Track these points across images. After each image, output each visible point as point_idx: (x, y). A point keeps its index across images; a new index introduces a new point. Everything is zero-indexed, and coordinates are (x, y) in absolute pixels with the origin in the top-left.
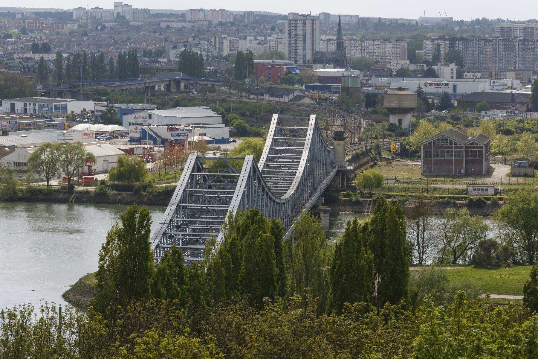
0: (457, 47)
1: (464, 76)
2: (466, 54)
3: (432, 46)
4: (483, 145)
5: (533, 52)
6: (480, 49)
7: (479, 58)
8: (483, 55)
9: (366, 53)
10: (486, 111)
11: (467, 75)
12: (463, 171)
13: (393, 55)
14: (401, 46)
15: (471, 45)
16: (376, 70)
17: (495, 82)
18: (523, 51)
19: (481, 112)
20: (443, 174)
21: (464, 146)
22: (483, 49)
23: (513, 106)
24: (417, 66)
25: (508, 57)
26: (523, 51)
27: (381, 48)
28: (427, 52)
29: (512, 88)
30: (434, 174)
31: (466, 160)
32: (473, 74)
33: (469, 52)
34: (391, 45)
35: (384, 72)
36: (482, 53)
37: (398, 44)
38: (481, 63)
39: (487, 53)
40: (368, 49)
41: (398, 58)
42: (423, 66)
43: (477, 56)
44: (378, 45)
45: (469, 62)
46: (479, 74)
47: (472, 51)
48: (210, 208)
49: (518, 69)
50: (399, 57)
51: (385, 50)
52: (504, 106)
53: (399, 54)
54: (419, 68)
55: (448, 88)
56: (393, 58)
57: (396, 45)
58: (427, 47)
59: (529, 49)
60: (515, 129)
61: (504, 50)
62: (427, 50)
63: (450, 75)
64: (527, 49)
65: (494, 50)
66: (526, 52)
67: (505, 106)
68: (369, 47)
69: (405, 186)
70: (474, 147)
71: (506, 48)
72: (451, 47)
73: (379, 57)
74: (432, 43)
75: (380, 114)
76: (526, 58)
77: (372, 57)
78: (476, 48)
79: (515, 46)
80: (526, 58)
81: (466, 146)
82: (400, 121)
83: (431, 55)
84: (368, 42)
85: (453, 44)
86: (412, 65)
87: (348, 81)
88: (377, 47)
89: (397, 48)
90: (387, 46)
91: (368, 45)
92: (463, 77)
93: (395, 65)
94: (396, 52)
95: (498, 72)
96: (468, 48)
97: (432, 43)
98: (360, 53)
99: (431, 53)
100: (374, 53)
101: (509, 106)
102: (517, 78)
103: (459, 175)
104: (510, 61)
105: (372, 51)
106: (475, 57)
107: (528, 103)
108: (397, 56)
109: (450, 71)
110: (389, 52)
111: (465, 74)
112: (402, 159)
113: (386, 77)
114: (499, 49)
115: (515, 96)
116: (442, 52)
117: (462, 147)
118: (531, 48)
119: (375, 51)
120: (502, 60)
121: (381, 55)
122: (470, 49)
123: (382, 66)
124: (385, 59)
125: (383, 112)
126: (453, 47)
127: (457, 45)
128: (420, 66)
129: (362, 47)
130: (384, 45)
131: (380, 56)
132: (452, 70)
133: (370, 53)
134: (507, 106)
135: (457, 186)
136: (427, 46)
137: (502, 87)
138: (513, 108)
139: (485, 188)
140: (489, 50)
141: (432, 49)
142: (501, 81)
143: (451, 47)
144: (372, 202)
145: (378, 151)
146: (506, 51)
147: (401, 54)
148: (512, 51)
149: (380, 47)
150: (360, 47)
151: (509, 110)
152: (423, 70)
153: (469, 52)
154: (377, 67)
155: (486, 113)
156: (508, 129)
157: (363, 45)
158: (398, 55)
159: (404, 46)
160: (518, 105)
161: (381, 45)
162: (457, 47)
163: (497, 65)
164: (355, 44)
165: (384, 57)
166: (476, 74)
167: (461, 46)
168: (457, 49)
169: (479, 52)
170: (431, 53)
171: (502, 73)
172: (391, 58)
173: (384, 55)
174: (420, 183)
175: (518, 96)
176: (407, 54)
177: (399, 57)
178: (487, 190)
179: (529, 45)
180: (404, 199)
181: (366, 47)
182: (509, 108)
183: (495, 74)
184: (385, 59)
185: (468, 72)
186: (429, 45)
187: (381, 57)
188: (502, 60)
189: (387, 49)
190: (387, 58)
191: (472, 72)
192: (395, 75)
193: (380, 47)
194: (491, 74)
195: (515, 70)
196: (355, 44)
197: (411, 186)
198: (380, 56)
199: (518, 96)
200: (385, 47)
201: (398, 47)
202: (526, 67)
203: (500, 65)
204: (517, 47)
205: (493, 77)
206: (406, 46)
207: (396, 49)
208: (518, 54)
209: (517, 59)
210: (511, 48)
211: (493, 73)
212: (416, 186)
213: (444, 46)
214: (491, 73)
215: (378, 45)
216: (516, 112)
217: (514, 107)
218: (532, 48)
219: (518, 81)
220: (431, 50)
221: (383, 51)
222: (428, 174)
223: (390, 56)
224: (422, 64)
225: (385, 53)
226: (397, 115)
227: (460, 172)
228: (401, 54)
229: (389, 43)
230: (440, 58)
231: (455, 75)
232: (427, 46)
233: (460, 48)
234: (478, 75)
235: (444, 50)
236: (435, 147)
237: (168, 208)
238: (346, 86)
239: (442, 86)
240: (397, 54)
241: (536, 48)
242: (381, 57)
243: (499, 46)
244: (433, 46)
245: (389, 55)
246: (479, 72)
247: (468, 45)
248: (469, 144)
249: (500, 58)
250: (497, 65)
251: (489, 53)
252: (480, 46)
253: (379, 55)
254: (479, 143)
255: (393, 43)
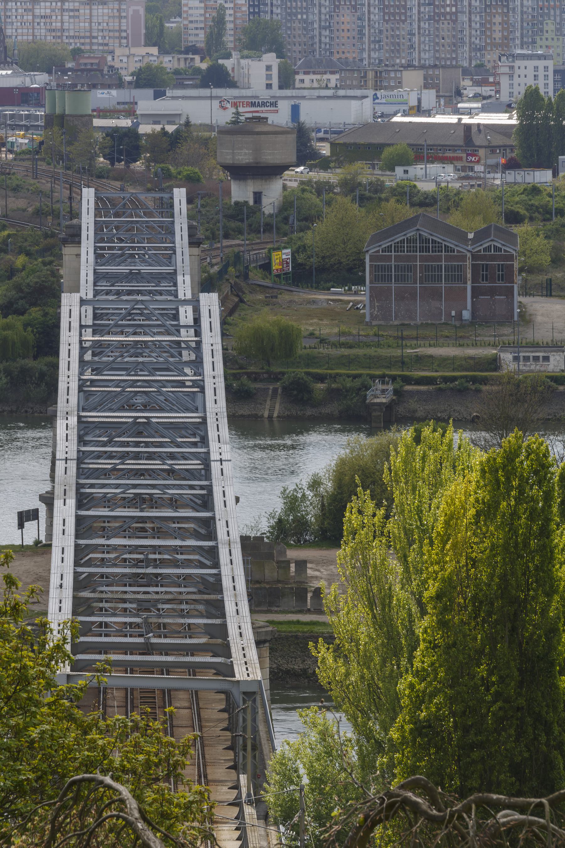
0: (267, 12)
1: (297, 82)
2: (290, 28)
3: (202, 12)
4: (514, 253)
5: (455, 21)
6: (323, 17)
7: (323, 39)
8: (331, 31)
9: (43, 31)
10: (406, 168)
11: (302, 81)
12: (466, 315)
13: (111, 34)
14: (131, 13)
15: (301, 8)
16: (82, 71)
17: (379, 96)
18: (429, 19)
19: (393, 170)
20: (419, 322)
21: (469, 255)
22: (331, 16)
23: (468, 155)
24: (179, 59)
25: (392, 36)
26: (429, 19)
27: (82, 18)
28: (191, 26)
29: (419, 110)
30: (396, 323)
31: (473, 288)
32: (318, 77)
33: (296, 25)
34: (106, 11)
35: (103, 75)
36: (330, 26)
37: (124, 7)
38: (326, 50)
39: (343, 27)
40: (48, 20)
41: (124, 41)
42: (192, 59)
43: (316, 32)
44: (72, 10)
45: (298, 48)
46: (334, 79)
47: (305, 21)
48: (154, 420)
49: (417, 64)
50: (125, 38)
51: (91, 22)
52: (446, 155)
53: (126, 31)
54: (182, 65)
55: (277, 111)
56: (111, 41)
57: (119, 10)
58: (191, 15)
59: (444, 15)
60: (527, 210)
61: (384, 20)
62: (191, 22)
63: (264, 82)
64: (439, 15)
65: (359, 19)
66: (438, 22)
67: (449, 154)
68: (51, 17)
69: (345, 352)
70: (493, 258)
71: (389, 14)
72: (254, 13)
73: (77, 41)
74: (202, 5)
75: (177, 178)
76: (437, 36)
77: (59, 41)
78: (313, 14)
79: (411, 9)
80: (437, 36)
81: (472, 255)
82: (258, 197)
83: (202, 36)
84: (48, 4)
85: (258, 6)
86: (167, 58)
87: (63, 98)
88: (70, 17)
89: (120, 17)
90: (95, 13)
91: (48, 11)
92: (294, 84)
93: (125, 60)
94: (117, 28)
95: (381, 72)
96: (296, 15)
97: (202, 5)
98: (31, 31)
99: (201, 28)
100: (63, 30)
101: (459, 154)
102: (426, 87)
103: (458, 324)
104: (399, 45)
105: (59, 24)
106: (312, 38)
107: (512, 148)
108: (120, 38)
109: (264, 72)
110: (100, 28)
111: (298, 77)
112: (298, 286)
113: (109, 87)
114: (372, 17)
115: (474, 130)
116: (230, 26)
117: (463, 258)
118: (448, 13)
119: (66, 26)
120: (379, 41)
121: (82, 34)
122: (299, 17)
123: (97, 61)
124: (91, 44)
125: (185, 173)
126: (259, 13)
127: (268, 9)
128: (186, 59)
129: (34, 16)
130: (88, 11)
131: (79, 37)
132: (269, 68)
133: (54, 30)
134: (455, 155)
135: (471, 352)
136: (191, 12)
137: (394, 108)
138: (470, 158)
139: (541, 354)
140: (347, 19)
141: (202, 19)
142: (392, 93)
143: (254, 13)
144: (280, 391)
145: (242, 268)
146: (387, 22)
147: (129, 31)
148: (404, 22)
149: (78, 17)
150: (30, 18)
151: (459, 165)
152: (198, 71)
153: (296, 25)
154: (85, 64)
155: (406, 172)
156: (512, 212)
157: (37, 12)
158: (124, 34)
159: (136, 12)
160: (482, 152)
161: (82, 11)
162: (267, 12)
163: (365, 55)
164: (16, 10)
165: (88, 41)
166: (325, 77)
167: (279, 11)
168: (268, 17)
169: (323, 24)
170: (201, 28)
171: (392, 75)
172: (106, 42)
173: (88, 34)
174: (379, 345)
175: (479, 131)
176: (143, 31)
177: (125, 38)
178: (546, 359)
179: (443, 7)
180: (358, 383)
181: (45, 17)
182: (460, 159)
183: (376, 77)
184: (91, 44)
185: (306, 73)
186: (197, 8)
187: (82, 41)
188: (379, 41)
189: (95, 19)
190: (95, 41)
191: (314, 73)
192: (130, 83)
193: (78, 17)
194: (365, 76)
195: (422, 67)
196: (16, 10)
197: (360, 352)
198: (79, 37)
199: (479, 131)
200: (91, 15)
201: (123, 14)
202: (437, 58)
203: (372, 54)
204: (415, 11)
205: (370, 83)
206: (142, 11)
207: (117, 20)
208: (416, 27)
209: (416, 39)
210: (400, 14)
211: (371, 75)
212: (371, 351)
213: (232, 12)
214: (366, 73)
215: (72, 10)
216: (479, 168)
217: (472, 155)
218: (451, 13)
219: (433, 92)
220: (201, 22)
221: (87, 24)
222: (382, 323)
223: (104, 37)
224: (191, 56)
225: (91, 30)
226: (250, 182)
227: (459, 316)
228: (129, 31)
229: (101, 7)
230: (224, 39)
231: (275, 81)
232: (191, 12)
233: (275, 16)
234: (329, 80)
235: (234, 22)
236: (422, 259)
237: (60, 424)
238: (58, 111)
239: (263, 109)
240: (120, 31)
241: (461, 12)
242: (82, 41)
243: (372, 9)
244: (205, 12)
245: (101, 34)
246: (332, 73)
247: (296, 8)
248: (480, 251)
249: (372, 39)
250: (365, 55)
251: (346, 27)
252: (323, 10)
253: (77, 34)
254: (503, 248)
255: (111, 6)
